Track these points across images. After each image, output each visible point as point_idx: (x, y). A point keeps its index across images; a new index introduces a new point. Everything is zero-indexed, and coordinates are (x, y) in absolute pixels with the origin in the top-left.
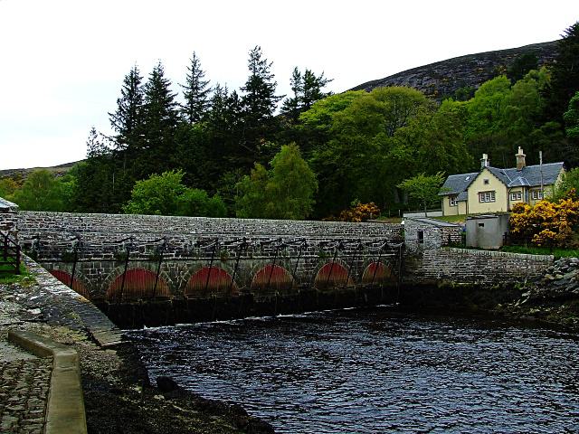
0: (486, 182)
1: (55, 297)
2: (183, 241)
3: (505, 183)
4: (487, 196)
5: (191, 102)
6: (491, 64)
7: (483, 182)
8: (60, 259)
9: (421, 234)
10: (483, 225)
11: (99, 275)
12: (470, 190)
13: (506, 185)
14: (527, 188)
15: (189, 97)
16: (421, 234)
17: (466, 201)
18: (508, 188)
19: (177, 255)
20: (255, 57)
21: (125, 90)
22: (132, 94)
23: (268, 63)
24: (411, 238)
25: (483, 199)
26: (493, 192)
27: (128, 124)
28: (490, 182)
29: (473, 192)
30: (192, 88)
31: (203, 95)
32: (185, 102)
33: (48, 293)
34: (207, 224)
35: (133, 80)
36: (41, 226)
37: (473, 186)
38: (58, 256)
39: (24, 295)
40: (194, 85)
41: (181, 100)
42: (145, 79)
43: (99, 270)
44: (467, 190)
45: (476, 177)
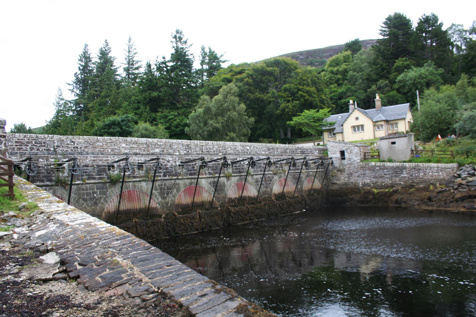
0: (357, 119)
1: (74, 231)
2: (169, 161)
3: (371, 118)
4: (358, 128)
5: (128, 74)
6: (307, 57)
7: (354, 119)
8: (53, 183)
9: (342, 153)
10: (394, 143)
11: (94, 198)
12: (345, 125)
13: (372, 120)
14: (387, 121)
15: (127, 70)
16: (342, 153)
17: (342, 133)
18: (373, 122)
19: (165, 176)
20: (178, 38)
21: (57, 95)
22: (85, 69)
23: (189, 43)
24: (334, 155)
25: (355, 130)
26: (362, 126)
27: (83, 91)
28: (359, 118)
29: (347, 127)
30: (129, 64)
31: (137, 68)
32: (124, 74)
33: (62, 224)
34: (188, 145)
35: (86, 57)
36: (31, 149)
37: (346, 122)
38: (50, 180)
39: (24, 230)
40: (131, 62)
41: (121, 73)
42: (95, 57)
43: (94, 193)
44: (342, 125)
45: (348, 118)
